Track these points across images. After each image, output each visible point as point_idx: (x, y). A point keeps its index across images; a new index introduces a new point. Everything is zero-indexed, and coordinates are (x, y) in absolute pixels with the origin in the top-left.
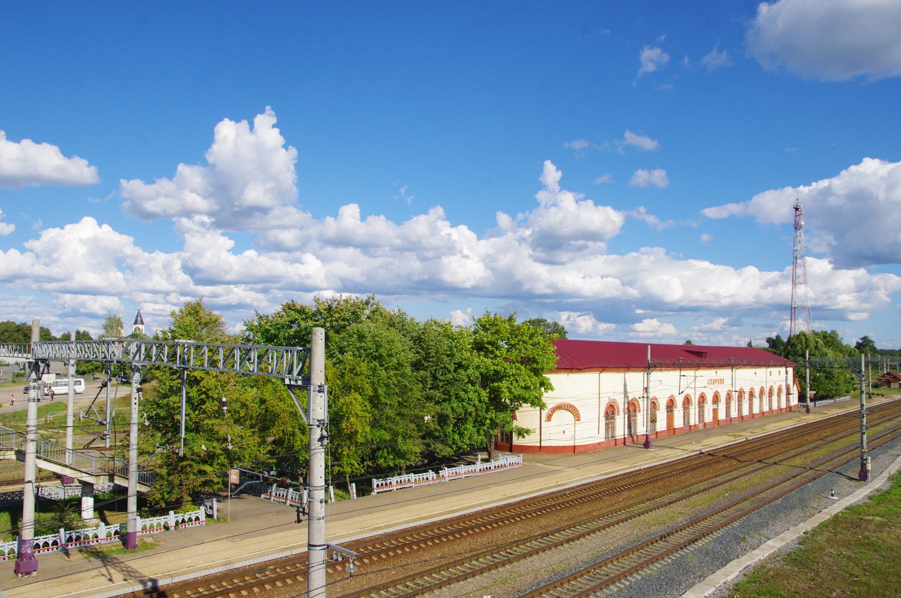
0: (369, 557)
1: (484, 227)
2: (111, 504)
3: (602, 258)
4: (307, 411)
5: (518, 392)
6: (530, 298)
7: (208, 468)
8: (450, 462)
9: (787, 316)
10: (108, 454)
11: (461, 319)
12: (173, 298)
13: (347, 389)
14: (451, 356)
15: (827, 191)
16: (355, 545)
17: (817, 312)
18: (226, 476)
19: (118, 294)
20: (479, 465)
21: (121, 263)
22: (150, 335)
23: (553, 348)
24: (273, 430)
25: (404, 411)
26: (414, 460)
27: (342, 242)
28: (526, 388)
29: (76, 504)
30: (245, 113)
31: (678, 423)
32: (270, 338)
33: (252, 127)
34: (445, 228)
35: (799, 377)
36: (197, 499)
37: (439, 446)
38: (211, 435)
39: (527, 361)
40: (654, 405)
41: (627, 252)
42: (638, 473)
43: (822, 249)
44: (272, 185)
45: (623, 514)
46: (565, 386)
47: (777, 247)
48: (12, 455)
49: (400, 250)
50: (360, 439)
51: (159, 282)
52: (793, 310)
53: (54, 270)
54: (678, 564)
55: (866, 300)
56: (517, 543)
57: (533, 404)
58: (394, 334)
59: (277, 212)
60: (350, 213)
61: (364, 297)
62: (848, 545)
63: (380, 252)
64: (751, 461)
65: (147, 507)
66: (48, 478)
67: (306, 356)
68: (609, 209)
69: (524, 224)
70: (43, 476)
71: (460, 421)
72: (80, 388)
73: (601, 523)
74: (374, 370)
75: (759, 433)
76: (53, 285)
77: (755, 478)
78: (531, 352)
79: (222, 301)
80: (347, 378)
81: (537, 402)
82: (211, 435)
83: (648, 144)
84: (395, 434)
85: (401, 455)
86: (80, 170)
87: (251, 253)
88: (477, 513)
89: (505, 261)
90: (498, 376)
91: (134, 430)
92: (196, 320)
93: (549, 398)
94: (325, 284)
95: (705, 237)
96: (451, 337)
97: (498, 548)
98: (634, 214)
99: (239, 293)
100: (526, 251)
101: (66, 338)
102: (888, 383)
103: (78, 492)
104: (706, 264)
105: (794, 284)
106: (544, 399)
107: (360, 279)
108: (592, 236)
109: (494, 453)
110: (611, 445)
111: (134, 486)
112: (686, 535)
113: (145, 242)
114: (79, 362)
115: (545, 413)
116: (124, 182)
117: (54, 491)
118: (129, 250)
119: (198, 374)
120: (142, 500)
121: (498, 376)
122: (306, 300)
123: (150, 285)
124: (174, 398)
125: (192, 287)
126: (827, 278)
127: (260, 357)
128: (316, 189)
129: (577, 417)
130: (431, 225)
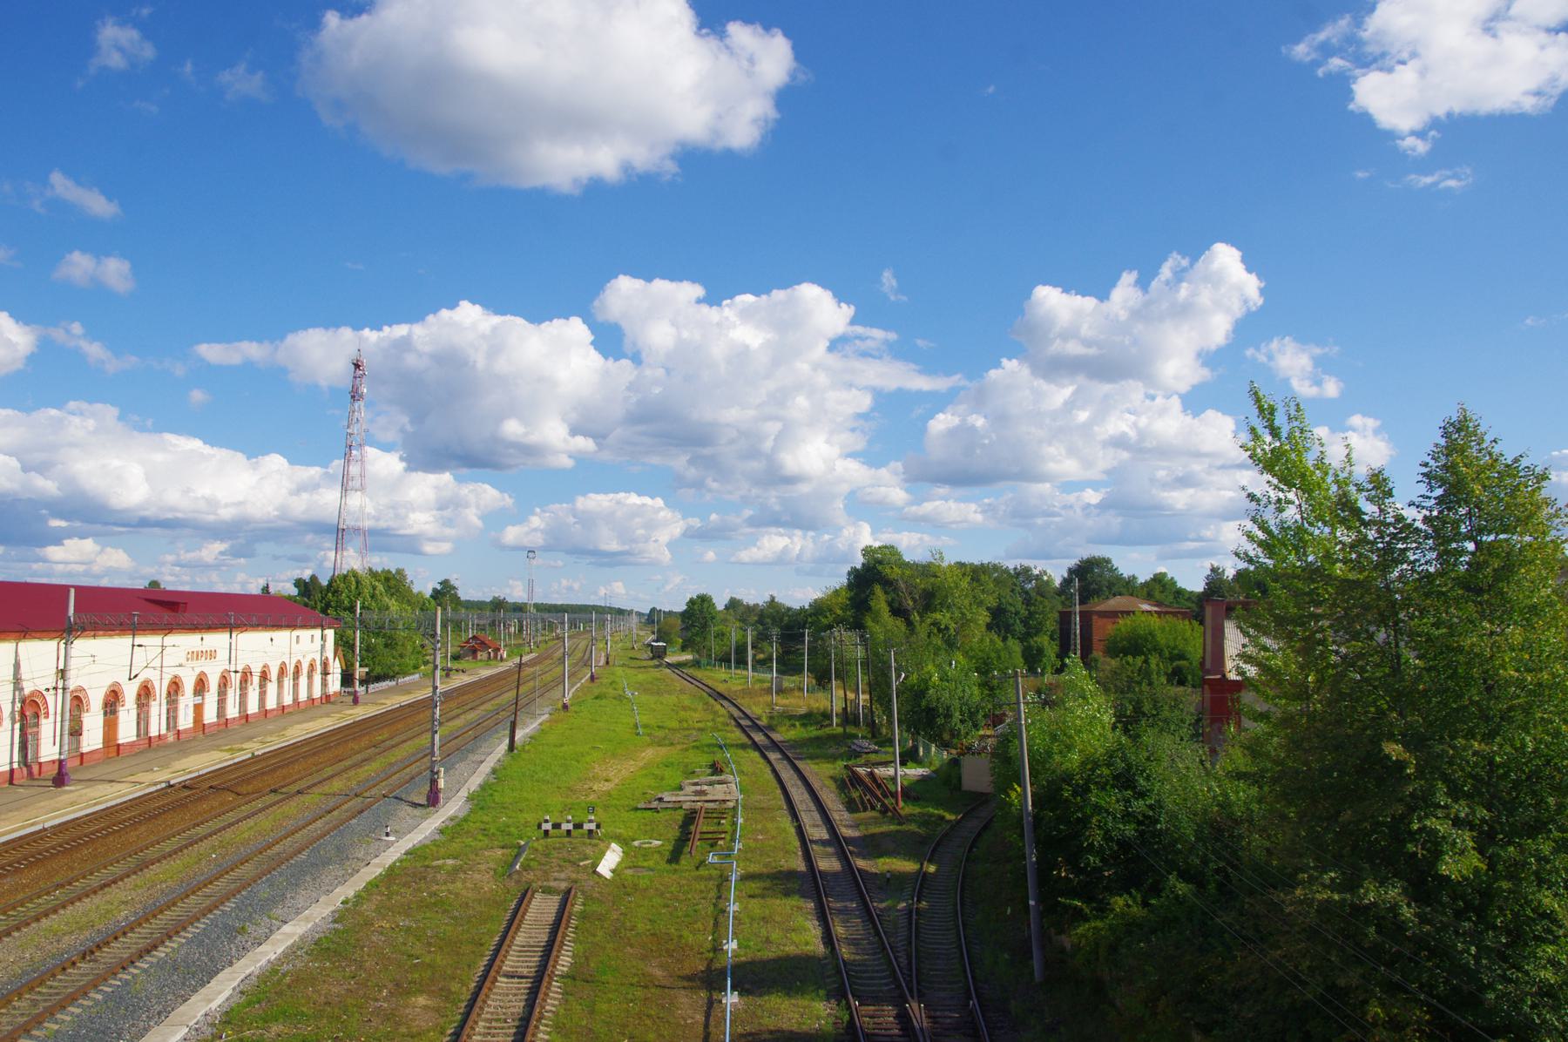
9: (330, 544)
15: (405, 344)
17: (377, 538)
35: (344, 644)
40: (78, 702)
43: (391, 436)
47: (316, 425)
52: (340, 534)
55: (449, 522)
62: (406, 911)
64: (259, 793)
77: (264, 822)
95: (197, 395)
98: (58, 334)
104: (196, 444)
105: (345, 489)
112: (135, 940)
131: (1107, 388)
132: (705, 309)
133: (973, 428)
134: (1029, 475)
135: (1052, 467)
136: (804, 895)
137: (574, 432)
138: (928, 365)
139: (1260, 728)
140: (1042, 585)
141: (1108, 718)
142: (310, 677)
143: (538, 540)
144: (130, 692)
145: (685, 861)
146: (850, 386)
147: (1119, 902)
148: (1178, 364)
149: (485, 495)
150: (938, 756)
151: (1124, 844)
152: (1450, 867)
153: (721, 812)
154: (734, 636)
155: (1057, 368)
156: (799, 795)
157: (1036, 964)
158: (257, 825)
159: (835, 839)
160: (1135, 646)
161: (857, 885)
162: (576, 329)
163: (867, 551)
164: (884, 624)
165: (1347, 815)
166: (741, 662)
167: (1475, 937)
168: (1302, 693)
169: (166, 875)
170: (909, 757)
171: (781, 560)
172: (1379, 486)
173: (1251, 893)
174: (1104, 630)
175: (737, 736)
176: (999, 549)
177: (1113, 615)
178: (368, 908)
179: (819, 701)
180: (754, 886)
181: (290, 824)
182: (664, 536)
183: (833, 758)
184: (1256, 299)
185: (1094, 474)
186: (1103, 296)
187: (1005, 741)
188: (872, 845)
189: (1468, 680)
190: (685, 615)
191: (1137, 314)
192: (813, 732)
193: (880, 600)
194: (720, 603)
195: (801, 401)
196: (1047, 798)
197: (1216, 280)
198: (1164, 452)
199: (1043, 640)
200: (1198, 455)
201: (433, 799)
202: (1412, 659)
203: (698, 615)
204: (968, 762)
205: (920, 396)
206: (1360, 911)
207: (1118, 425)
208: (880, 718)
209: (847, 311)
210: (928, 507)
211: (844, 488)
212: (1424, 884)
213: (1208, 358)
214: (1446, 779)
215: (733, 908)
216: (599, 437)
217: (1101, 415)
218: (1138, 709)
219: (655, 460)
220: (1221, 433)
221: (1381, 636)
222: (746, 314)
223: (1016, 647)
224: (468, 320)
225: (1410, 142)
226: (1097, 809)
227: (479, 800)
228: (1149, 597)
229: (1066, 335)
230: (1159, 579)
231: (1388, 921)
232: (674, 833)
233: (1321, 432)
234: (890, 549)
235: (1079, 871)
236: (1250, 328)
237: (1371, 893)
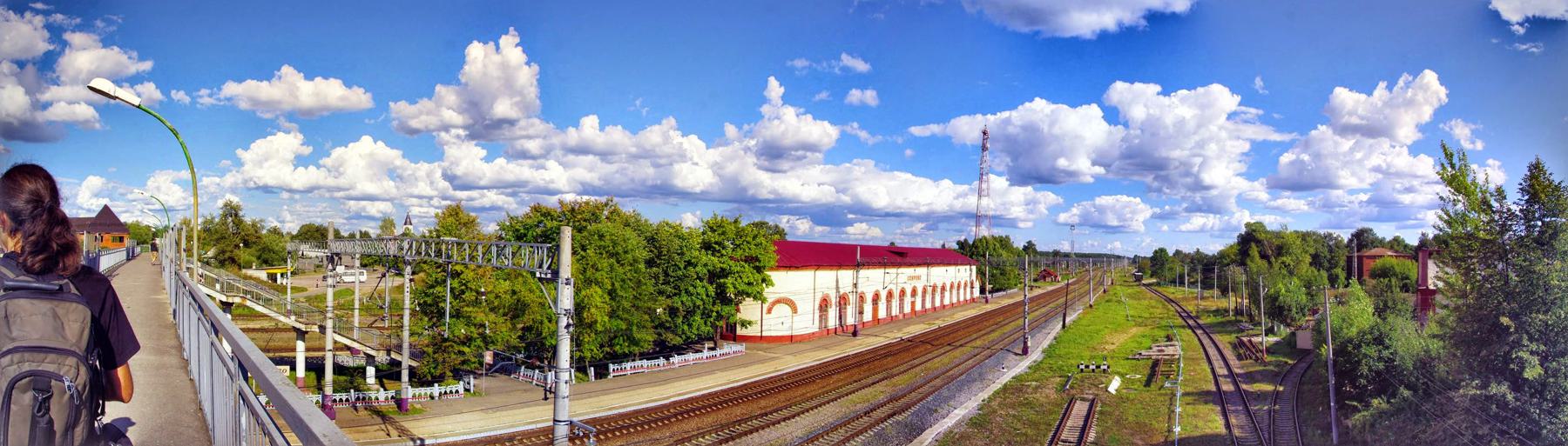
0: (605, 433)
1: (713, 138)
2: (388, 374)
3: (819, 168)
4: (555, 302)
5: (742, 287)
6: (753, 202)
7: (466, 350)
8: (680, 350)
9: (973, 223)
10: (386, 333)
11: (691, 220)
12: (435, 202)
13: (589, 282)
14: (682, 254)
15: (1007, 121)
16: (593, 422)
17: (996, 220)
18: (482, 356)
19: (390, 200)
20: (706, 353)
21: (393, 173)
22: (418, 235)
23: (773, 248)
24: (525, 318)
25: (640, 304)
26: (648, 347)
27: (582, 150)
28: (749, 284)
29: (361, 371)
30: (490, 35)
31: (882, 314)
32: (520, 237)
33: (498, 48)
34: (677, 137)
35: (981, 273)
36: (458, 375)
37: (670, 336)
38: (469, 322)
39: (750, 260)
40: (862, 298)
41: (842, 162)
42: (847, 358)
43: (1002, 168)
44: (518, 99)
45: (833, 395)
46: (785, 282)
47: (965, 164)
48: (316, 329)
49: (635, 157)
50: (599, 327)
51: (423, 188)
52: (978, 218)
53: (342, 182)
54: (879, 435)
55: (1031, 212)
56: (739, 422)
57: (755, 298)
58: (629, 232)
59: (523, 123)
60: (590, 123)
61: (604, 199)
62: (1013, 406)
63: (616, 158)
64: (942, 345)
65: (417, 379)
66: (341, 349)
67: (555, 252)
68: (826, 123)
69: (750, 134)
70: (339, 347)
71: (690, 313)
72: (364, 278)
73: (814, 403)
74: (611, 266)
75: (949, 321)
76: (341, 194)
77: (945, 359)
78: (754, 252)
79: (476, 204)
80: (589, 273)
81: (758, 297)
82: (469, 322)
83: (861, 66)
84: (630, 324)
85: (634, 342)
86: (359, 98)
87: (501, 161)
88: (704, 396)
89: (731, 168)
90: (724, 273)
91: (407, 313)
92: (456, 219)
93: (770, 293)
94: (566, 188)
95: (909, 152)
96: (681, 237)
97: (722, 427)
98: (848, 129)
99: (492, 197)
100: (751, 159)
101: (352, 236)
102: (1044, 278)
103: (363, 362)
104: (909, 176)
105: (980, 196)
106: (765, 294)
107: (597, 183)
108: (811, 147)
109: (720, 342)
110: (825, 332)
111: (406, 361)
112: (886, 410)
113: (413, 155)
114: (363, 256)
115: (766, 306)
116: (392, 104)
117: (346, 360)
118: (399, 162)
119: (458, 268)
120: (412, 371)
121: (724, 273)
122: (551, 202)
123: (416, 192)
124: (439, 289)
125: (451, 192)
126: (1004, 193)
127: (514, 254)
128: (557, 105)
129: (795, 310)
130: (662, 135)
131: (1371, 141)
132: (1161, 97)
133: (1302, 162)
134: (1331, 185)
135: (1342, 182)
136: (1215, 403)
137: (1094, 164)
138: (1279, 127)
139: (1443, 312)
140: (1338, 243)
141: (1371, 310)
142: (901, 300)
143: (1076, 220)
144: (883, 295)
145: (1152, 386)
146: (1238, 138)
147: (1375, 402)
148: (1407, 132)
149: (1049, 197)
150: (1284, 331)
151: (1378, 373)
152: (1529, 374)
153: (1172, 361)
154: (1178, 270)
155: (1345, 130)
156: (1212, 351)
157: (1334, 435)
158: (941, 360)
159: (1231, 374)
160: (1384, 273)
161: (1244, 398)
162: (1094, 110)
163: (1247, 225)
164: (1256, 263)
165: (1484, 352)
166: (1182, 283)
167: (1539, 405)
168: (1464, 295)
169: (902, 381)
170: (1270, 331)
171: (1202, 230)
172: (1500, 194)
173: (1439, 393)
174: (1370, 265)
175: (1180, 321)
176: (1314, 223)
177: (1374, 257)
178: (994, 404)
179: (1222, 303)
180: (1189, 399)
181: (920, 381)
182: (1141, 218)
183: (1231, 333)
184: (1445, 99)
185: (1365, 186)
186: (1370, 94)
187: (1319, 322)
188: (1251, 377)
189: (1538, 286)
190: (1152, 259)
191: (1386, 104)
192: (1219, 319)
193: (1254, 251)
194: (1171, 253)
195: (1213, 147)
196: (1340, 351)
197: (1425, 88)
198: (1399, 175)
199: (1338, 271)
200: (1416, 177)
201: (1025, 351)
202: (1512, 275)
203: (1159, 258)
204: (1299, 333)
205: (1276, 144)
206: (1489, 398)
207: (1376, 160)
208: (1255, 312)
209: (1237, 99)
210: (1279, 202)
211: (1236, 192)
212: (1517, 383)
213: (1421, 128)
214: (1527, 333)
215: (1178, 410)
216: (1107, 166)
217: (1367, 157)
218: (1386, 305)
219: (1136, 178)
220: (1426, 166)
221: (1500, 266)
222: (1183, 100)
223: (1324, 274)
224: (1039, 109)
225: (1517, 27)
226: (1365, 356)
227: (1049, 352)
228: (1392, 248)
229: (1351, 114)
230: (1396, 239)
231: (1502, 403)
232: (1147, 371)
233: (1474, 167)
234: (1260, 224)
235: (1355, 387)
236: (1442, 114)
237: (1494, 389)
